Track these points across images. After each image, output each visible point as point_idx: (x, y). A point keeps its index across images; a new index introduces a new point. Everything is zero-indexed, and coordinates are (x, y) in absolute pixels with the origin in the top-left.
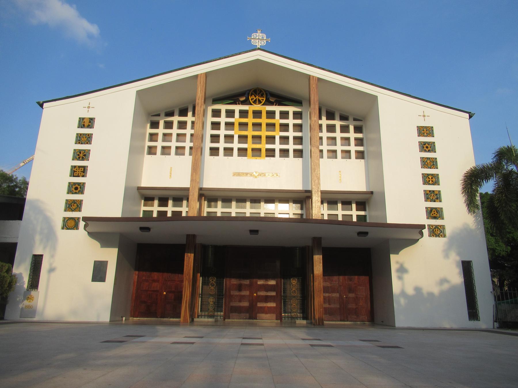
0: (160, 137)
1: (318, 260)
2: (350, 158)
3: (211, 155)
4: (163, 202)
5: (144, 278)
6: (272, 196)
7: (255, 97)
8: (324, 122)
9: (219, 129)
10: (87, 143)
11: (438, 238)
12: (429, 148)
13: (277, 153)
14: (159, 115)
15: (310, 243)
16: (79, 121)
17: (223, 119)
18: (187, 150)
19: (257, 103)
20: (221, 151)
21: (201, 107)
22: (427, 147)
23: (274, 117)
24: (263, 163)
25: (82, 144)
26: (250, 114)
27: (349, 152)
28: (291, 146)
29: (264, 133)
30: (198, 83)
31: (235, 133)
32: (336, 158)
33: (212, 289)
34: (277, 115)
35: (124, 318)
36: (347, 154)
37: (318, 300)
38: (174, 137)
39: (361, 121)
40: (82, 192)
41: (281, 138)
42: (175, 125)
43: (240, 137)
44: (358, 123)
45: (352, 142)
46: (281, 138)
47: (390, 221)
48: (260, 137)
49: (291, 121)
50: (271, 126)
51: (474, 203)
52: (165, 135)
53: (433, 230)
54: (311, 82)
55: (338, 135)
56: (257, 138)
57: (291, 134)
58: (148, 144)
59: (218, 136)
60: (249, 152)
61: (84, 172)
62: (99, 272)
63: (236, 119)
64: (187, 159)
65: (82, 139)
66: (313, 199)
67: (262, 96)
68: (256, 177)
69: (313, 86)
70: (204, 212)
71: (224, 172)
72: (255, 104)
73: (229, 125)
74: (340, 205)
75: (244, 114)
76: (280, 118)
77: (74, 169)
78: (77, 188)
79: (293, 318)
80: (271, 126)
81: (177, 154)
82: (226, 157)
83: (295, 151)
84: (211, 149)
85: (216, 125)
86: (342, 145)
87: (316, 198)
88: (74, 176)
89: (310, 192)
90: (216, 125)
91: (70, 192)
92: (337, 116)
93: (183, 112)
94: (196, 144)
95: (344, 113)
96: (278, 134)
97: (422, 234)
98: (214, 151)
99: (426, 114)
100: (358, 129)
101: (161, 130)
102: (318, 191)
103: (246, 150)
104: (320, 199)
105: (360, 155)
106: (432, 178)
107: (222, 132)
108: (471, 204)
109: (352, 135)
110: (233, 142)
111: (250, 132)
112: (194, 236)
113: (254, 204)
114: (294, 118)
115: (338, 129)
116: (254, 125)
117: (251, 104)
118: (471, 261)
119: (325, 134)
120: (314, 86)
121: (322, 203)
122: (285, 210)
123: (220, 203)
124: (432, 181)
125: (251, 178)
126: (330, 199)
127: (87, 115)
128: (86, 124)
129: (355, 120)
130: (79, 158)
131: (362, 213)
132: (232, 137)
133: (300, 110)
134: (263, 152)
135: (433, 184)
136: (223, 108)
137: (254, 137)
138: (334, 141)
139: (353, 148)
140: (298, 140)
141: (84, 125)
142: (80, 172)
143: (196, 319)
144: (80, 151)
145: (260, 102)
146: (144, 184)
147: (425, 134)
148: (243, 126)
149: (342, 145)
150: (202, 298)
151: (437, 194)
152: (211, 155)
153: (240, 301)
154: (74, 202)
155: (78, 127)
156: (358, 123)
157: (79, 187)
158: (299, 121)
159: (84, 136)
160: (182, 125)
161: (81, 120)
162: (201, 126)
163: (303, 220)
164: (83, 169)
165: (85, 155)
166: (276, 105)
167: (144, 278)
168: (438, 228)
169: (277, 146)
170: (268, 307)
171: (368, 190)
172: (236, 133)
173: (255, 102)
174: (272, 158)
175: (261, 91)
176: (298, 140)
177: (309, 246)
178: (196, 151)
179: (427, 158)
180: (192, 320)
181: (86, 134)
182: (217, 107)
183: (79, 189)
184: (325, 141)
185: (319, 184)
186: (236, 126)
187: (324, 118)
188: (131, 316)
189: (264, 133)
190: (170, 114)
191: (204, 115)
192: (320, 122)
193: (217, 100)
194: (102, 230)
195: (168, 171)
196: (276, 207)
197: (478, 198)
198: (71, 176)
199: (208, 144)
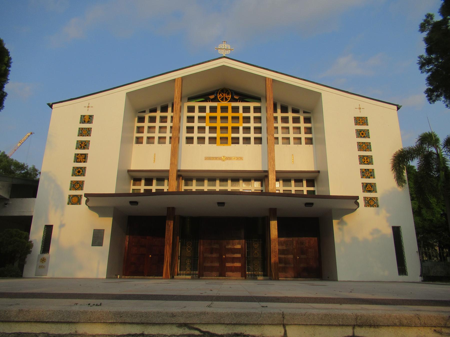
0: (146, 130)
1: (274, 224)
3: (187, 143)
4: (149, 182)
5: (133, 244)
7: (223, 95)
8: (279, 115)
10: (87, 136)
13: (241, 140)
14: (144, 112)
17: (196, 114)
18: (168, 140)
19: (224, 100)
20: (195, 140)
21: (178, 105)
22: (362, 134)
26: (219, 110)
27: (300, 139)
28: (252, 135)
29: (230, 124)
34: (241, 110)
35: (119, 276)
36: (298, 140)
38: (157, 129)
42: (158, 119)
43: (210, 128)
44: (307, 115)
45: (303, 130)
48: (227, 128)
49: (252, 115)
51: (402, 179)
52: (160, 127)
54: (267, 82)
55: (291, 125)
57: (252, 125)
60: (218, 140)
61: (85, 158)
62: (97, 238)
63: (208, 113)
64: (167, 147)
67: (228, 94)
68: (224, 161)
71: (200, 157)
72: (223, 101)
74: (293, 182)
75: (213, 109)
76: (205, 112)
80: (236, 119)
81: (159, 143)
83: (255, 138)
84: (187, 138)
85: (190, 119)
87: (272, 177)
88: (77, 162)
89: (267, 172)
90: (190, 119)
91: (74, 174)
92: (290, 110)
93: (164, 109)
94: (175, 134)
96: (241, 125)
98: (190, 140)
100: (307, 120)
101: (146, 124)
103: (215, 138)
105: (309, 141)
106: (367, 159)
107: (196, 124)
108: (399, 179)
109: (302, 125)
111: (219, 124)
112: (173, 209)
114: (254, 112)
115: (291, 120)
116: (222, 118)
119: (280, 125)
120: (269, 86)
123: (194, 182)
124: (367, 161)
125: (220, 161)
126: (285, 177)
127: (87, 113)
128: (87, 120)
129: (304, 112)
130: (81, 147)
132: (204, 128)
134: (230, 140)
135: (368, 164)
136: (197, 105)
139: (303, 136)
140: (258, 130)
141: (85, 121)
144: (82, 142)
145: (226, 99)
147: (361, 123)
148: (213, 119)
149: (294, 133)
150: (180, 259)
152: (187, 143)
154: (77, 182)
155: (80, 123)
156: (307, 115)
157: (81, 171)
159: (85, 130)
160: (164, 119)
161: (83, 117)
164: (84, 156)
165: (86, 145)
166: (239, 102)
167: (133, 244)
168: (372, 200)
169: (241, 135)
170: (234, 267)
172: (207, 125)
173: (222, 100)
174: (237, 145)
175: (227, 91)
178: (175, 140)
181: (87, 128)
182: (191, 104)
183: (81, 172)
186: (207, 119)
187: (279, 110)
189: (230, 124)
190: (154, 110)
191: (180, 111)
193: (190, 99)
194: (99, 203)
195: (153, 157)
199: (184, 134)
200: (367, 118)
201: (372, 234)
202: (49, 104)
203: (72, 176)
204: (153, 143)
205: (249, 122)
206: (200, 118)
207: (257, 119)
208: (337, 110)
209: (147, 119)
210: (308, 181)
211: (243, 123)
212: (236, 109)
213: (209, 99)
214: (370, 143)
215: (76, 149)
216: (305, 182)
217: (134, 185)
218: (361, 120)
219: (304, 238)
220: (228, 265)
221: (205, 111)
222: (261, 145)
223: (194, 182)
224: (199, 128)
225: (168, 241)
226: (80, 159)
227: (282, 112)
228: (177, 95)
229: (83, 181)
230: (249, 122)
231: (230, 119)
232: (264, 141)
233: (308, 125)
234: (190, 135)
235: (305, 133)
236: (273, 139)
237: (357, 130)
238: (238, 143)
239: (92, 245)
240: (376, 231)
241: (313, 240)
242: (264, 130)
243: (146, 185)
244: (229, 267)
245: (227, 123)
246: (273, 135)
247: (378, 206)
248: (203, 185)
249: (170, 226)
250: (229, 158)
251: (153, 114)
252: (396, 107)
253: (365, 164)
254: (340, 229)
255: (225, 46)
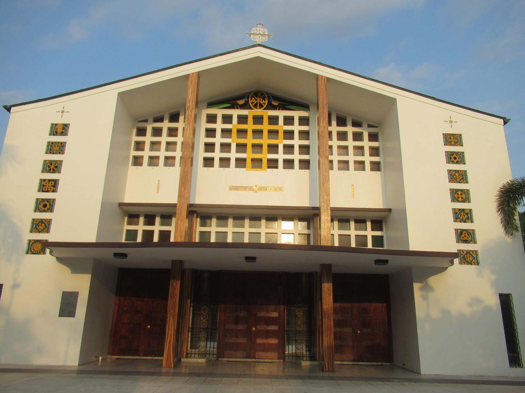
0: (147, 146)
1: (327, 288)
2: (364, 169)
3: (206, 165)
4: (150, 220)
6: (274, 215)
7: (256, 100)
8: (335, 128)
9: (214, 136)
10: (60, 153)
11: (470, 266)
12: (457, 159)
13: (281, 164)
14: (146, 121)
15: (318, 270)
16: (52, 127)
17: (219, 126)
18: (178, 161)
19: (258, 107)
20: (217, 162)
21: (192, 111)
22: (455, 158)
23: (277, 123)
24: (265, 176)
25: (53, 153)
26: (250, 120)
27: (363, 163)
29: (265, 141)
30: (189, 83)
31: (233, 141)
32: (348, 169)
33: (203, 322)
34: (281, 121)
35: (100, 358)
36: (360, 165)
37: (327, 340)
38: (163, 146)
39: (377, 127)
40: (51, 210)
41: (285, 146)
42: (165, 132)
43: (238, 145)
44: (373, 130)
45: (367, 151)
46: (285, 146)
47: (413, 247)
48: (261, 146)
49: (296, 128)
50: (273, 133)
51: (512, 224)
52: (168, 143)
53: (464, 257)
54: (320, 82)
55: (350, 143)
56: (257, 147)
57: (296, 142)
58: (134, 153)
59: (213, 145)
60: (249, 163)
63: (234, 125)
64: (175, 172)
65: (54, 148)
66: (322, 218)
67: (264, 99)
68: (256, 192)
69: (322, 87)
70: (195, 232)
71: (217, 187)
72: (256, 108)
73: (226, 132)
74: (352, 224)
75: (242, 119)
77: (43, 183)
78: (45, 205)
79: (299, 357)
80: (273, 133)
82: (222, 169)
83: (301, 161)
84: (205, 159)
85: (211, 133)
86: (355, 155)
87: (325, 217)
88: (43, 191)
89: (318, 209)
90: (211, 133)
92: (349, 122)
93: (174, 118)
94: (186, 154)
95: (355, 119)
96: (282, 142)
97: (452, 263)
98: (208, 162)
99: (453, 120)
100: (373, 137)
101: (148, 138)
102: (327, 209)
103: (244, 160)
104: (329, 219)
105: (376, 167)
106: (461, 194)
107: (218, 140)
108: (508, 223)
109: (366, 144)
110: (230, 152)
111: (250, 140)
112: (181, 262)
113: (253, 222)
114: (300, 124)
115: (350, 136)
116: (254, 132)
117: (252, 109)
118: (511, 294)
119: (335, 143)
120: (322, 87)
121: (332, 220)
122: (288, 233)
123: (214, 221)
124: (462, 198)
125: (251, 192)
126: (342, 217)
127: (61, 121)
128: (59, 131)
129: (369, 126)
130: (50, 170)
131: (378, 233)
132: (229, 145)
133: (307, 129)
134: (265, 163)
135: (463, 202)
136: (219, 112)
137: (254, 146)
138: (345, 150)
139: (367, 159)
140: (305, 149)
141: (56, 132)
142: (50, 187)
143: (184, 360)
144: (51, 162)
145: (261, 106)
146: (128, 199)
147: (453, 143)
148: (242, 133)
149: (355, 155)
150: (191, 332)
151: (467, 214)
152: (206, 165)
153: (237, 337)
154: (42, 221)
155: (50, 135)
156: (373, 130)
157: (48, 204)
158: (305, 128)
159: (57, 145)
160: (173, 132)
162: (191, 132)
163: (312, 246)
164: (53, 182)
165: (56, 167)
166: (279, 109)
168: (470, 254)
169: (281, 156)
170: (269, 344)
171: (385, 208)
172: (233, 141)
173: (255, 106)
174: (274, 170)
175: (262, 94)
176: (305, 149)
177: (316, 272)
179: (455, 171)
180: (178, 363)
181: (59, 143)
182: (212, 111)
183: (48, 206)
184: (335, 150)
185: (329, 200)
187: (334, 123)
188: (109, 354)
189: (265, 141)
191: (195, 121)
192: (330, 129)
193: (211, 105)
194: (71, 254)
195: (153, 185)
196: (280, 226)
197: (517, 217)
198: (39, 191)
199: (201, 154)
200: (461, 135)
201: (470, 305)
202: (5, 107)
203: (35, 211)
204: (157, 165)
205: (292, 138)
206: (224, 131)
207: (305, 135)
208: (420, 124)
209: (149, 131)
210: (373, 222)
211: (285, 139)
212: (274, 120)
213: (237, 104)
214: (466, 171)
215: (43, 172)
216: (369, 224)
217: (129, 224)
218: (452, 137)
219: (366, 305)
220: (259, 341)
221: (230, 122)
222: (307, 171)
223: (214, 221)
224: (222, 145)
225: (172, 311)
226: (47, 187)
227: (338, 125)
228: (191, 97)
229: (50, 220)
230: (292, 138)
231: (265, 133)
232: (314, 164)
233: (375, 144)
234: (209, 155)
235: (371, 155)
236: (327, 163)
237: (447, 153)
238: (276, 167)
239: (60, 316)
240: (477, 301)
241: (381, 306)
242: (314, 150)
243: (146, 224)
244: (261, 344)
245: (262, 138)
246: (328, 157)
247: (478, 264)
248: (226, 226)
249: (175, 289)
250: (263, 189)
251: (158, 125)
252: (501, 121)
253: (459, 201)
254: (425, 298)
255: (260, 30)
